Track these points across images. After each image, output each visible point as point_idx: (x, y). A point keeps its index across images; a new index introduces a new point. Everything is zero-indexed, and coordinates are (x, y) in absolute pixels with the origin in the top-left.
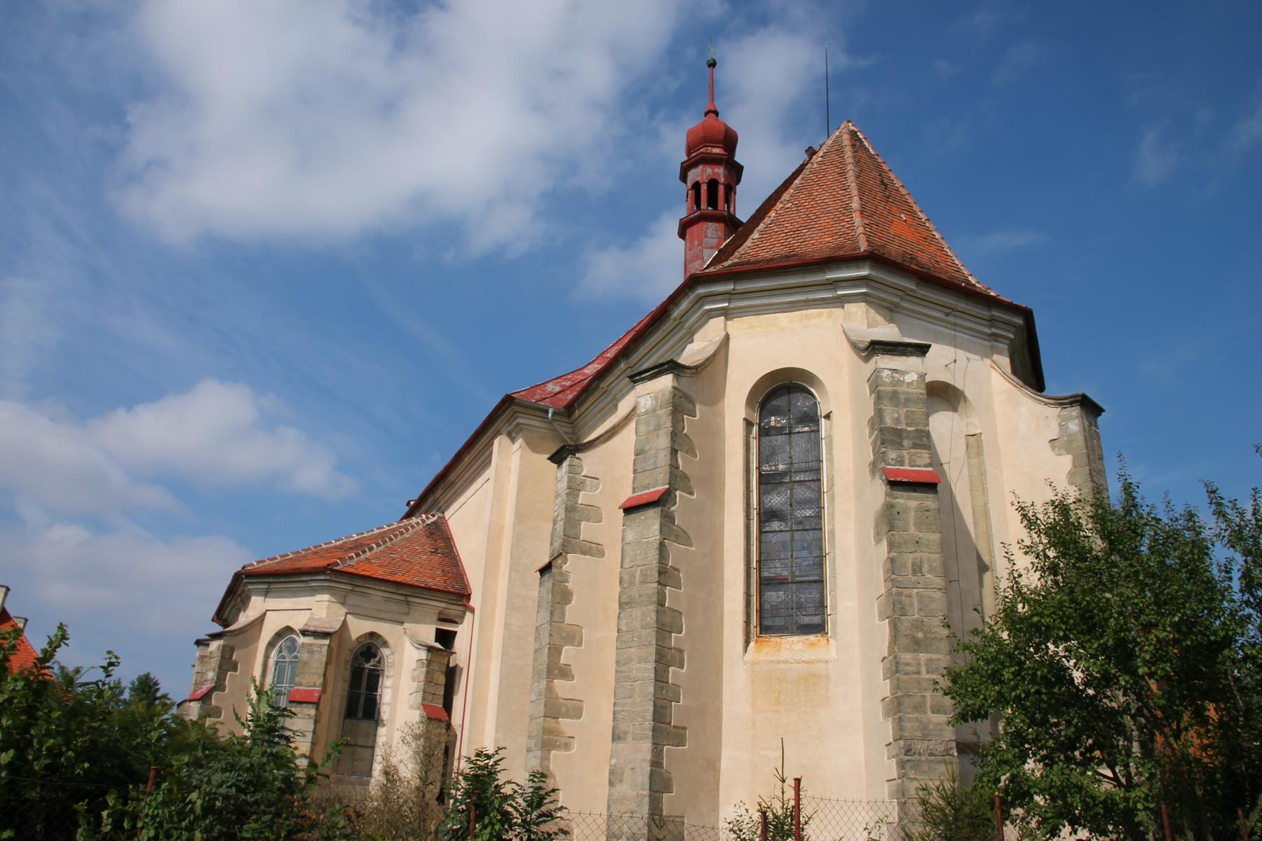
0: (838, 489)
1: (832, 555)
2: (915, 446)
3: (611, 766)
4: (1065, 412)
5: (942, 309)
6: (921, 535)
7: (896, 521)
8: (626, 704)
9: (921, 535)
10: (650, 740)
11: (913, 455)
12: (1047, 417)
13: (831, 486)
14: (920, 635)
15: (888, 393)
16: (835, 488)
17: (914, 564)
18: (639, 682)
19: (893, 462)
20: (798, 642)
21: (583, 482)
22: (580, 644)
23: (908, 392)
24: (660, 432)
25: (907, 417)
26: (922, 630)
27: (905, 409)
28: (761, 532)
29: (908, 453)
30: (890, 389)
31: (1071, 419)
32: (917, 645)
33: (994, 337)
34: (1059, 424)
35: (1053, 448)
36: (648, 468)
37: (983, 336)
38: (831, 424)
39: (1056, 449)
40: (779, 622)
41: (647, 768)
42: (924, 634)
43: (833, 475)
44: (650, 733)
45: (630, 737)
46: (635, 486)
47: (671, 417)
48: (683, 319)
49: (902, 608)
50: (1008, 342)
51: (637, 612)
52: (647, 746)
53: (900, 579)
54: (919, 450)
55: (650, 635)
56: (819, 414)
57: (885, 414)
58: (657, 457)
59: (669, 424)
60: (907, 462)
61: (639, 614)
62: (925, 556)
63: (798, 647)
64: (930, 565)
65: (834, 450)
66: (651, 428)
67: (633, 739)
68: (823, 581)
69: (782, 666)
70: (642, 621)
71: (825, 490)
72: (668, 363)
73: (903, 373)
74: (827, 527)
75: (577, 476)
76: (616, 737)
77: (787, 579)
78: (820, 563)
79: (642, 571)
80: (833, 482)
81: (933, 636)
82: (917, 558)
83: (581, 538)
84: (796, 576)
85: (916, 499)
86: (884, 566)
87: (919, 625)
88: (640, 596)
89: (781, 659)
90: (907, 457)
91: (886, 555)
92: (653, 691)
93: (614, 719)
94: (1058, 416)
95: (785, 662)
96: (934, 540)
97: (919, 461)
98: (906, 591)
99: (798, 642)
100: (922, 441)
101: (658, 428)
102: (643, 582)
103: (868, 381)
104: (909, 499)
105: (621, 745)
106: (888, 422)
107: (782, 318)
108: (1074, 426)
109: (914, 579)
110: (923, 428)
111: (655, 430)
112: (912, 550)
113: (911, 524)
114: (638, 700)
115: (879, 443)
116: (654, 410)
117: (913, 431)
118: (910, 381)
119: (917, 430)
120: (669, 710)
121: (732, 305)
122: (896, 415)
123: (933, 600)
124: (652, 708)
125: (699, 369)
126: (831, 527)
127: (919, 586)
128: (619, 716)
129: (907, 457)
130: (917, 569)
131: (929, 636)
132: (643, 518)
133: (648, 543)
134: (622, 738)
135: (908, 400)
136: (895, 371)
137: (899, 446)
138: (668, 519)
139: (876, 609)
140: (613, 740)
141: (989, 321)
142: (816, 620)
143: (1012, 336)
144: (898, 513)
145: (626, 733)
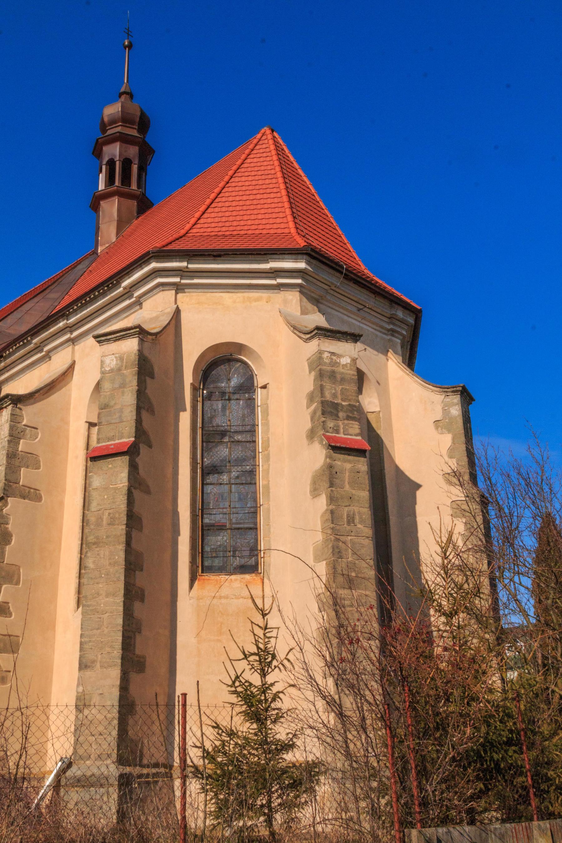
0: (272, 450)
1: (266, 506)
2: (348, 418)
3: (78, 693)
4: (448, 399)
5: (355, 304)
6: (354, 492)
7: (334, 480)
8: (94, 635)
9: (354, 492)
10: (119, 667)
11: (347, 425)
12: (433, 402)
13: (266, 447)
14: (353, 574)
15: (327, 372)
16: (271, 449)
17: (348, 516)
18: (107, 614)
19: (331, 430)
20: (236, 580)
21: (23, 431)
22: (18, 583)
23: (343, 373)
24: (125, 390)
25: (342, 393)
26: (355, 571)
27: (341, 387)
28: (203, 484)
29: (343, 423)
30: (329, 368)
31: (453, 405)
32: (351, 584)
33: (393, 332)
34: (442, 408)
35: (437, 428)
36: (113, 421)
37: (383, 331)
38: (268, 393)
39: (440, 429)
40: (217, 562)
41: (116, 693)
42: (356, 574)
43: (268, 438)
44: (119, 661)
45: (98, 665)
46: (100, 436)
47: (136, 377)
48: (132, 289)
49: (339, 552)
50: (401, 337)
51: (104, 552)
52: (115, 674)
53: (338, 527)
54: (351, 422)
55: (119, 572)
56: (256, 384)
57: (325, 389)
58: (122, 412)
59: (135, 383)
60: (342, 431)
61: (107, 553)
62: (356, 509)
63: (236, 585)
64: (361, 518)
65: (269, 417)
66: (117, 386)
67: (101, 667)
68: (256, 529)
69: (224, 601)
70: (110, 559)
71: (260, 451)
72: (135, 327)
73: (339, 356)
74: (261, 482)
75: (19, 425)
76: (83, 666)
77: (226, 526)
78: (255, 513)
79: (109, 514)
80: (269, 444)
81: (363, 576)
82: (350, 511)
83: (21, 483)
84: (234, 524)
85: (349, 462)
86: (322, 516)
87: (351, 566)
88: (107, 537)
89: (223, 595)
90: (342, 426)
91: (325, 507)
92: (122, 623)
93: (81, 649)
94: (443, 402)
95: (227, 597)
96: (364, 497)
97: (351, 431)
98: (342, 538)
99: (236, 580)
100: (354, 414)
101: (123, 386)
102: (111, 524)
103: (308, 360)
104: (345, 461)
105: (88, 673)
106: (328, 396)
107: (227, 297)
108: (456, 411)
109: (348, 528)
110: (354, 404)
111: (120, 387)
112: (347, 504)
113: (346, 483)
114: (106, 631)
115: (319, 413)
116: (119, 370)
117: (347, 405)
118: (345, 363)
119: (349, 404)
120: (133, 640)
121: (183, 281)
122: (334, 391)
123: (363, 546)
124: (121, 638)
125: (158, 336)
126: (265, 483)
127: (353, 534)
128: (86, 646)
129: (342, 426)
130: (351, 520)
131: (360, 575)
132: (110, 466)
133: (116, 489)
134: (89, 667)
135: (343, 380)
136: (333, 354)
137: (337, 417)
138: (133, 468)
139: (311, 552)
140: (80, 669)
141: (389, 318)
142: (252, 561)
143: (404, 333)
144: (336, 473)
145: (93, 662)
